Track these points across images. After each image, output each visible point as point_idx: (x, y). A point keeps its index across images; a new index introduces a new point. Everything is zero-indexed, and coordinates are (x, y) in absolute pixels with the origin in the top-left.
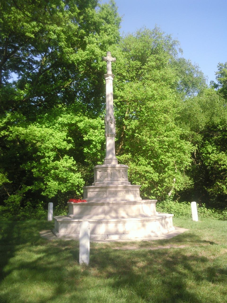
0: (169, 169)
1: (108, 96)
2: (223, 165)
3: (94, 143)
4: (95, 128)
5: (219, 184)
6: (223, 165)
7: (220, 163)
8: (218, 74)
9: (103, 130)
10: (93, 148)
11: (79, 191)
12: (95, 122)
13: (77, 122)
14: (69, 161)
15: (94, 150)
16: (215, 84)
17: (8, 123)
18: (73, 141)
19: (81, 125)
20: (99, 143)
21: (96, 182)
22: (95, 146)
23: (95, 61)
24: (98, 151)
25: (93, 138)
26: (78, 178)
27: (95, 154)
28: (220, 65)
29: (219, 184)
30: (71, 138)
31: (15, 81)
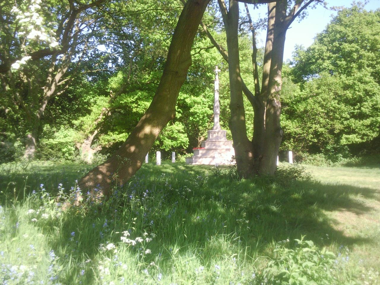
0: (249, 132)
1: (216, 102)
2: (289, 129)
3: (198, 114)
4: (198, 103)
5: (286, 143)
6: (289, 129)
7: (286, 128)
8: (294, 53)
9: (204, 105)
10: (197, 117)
11: (185, 146)
12: (198, 99)
13: (185, 98)
14: (179, 125)
15: (198, 119)
16: (291, 62)
17: (139, 99)
18: (182, 112)
19: (188, 101)
20: (201, 114)
21: (208, 140)
22: (198, 116)
23: (241, 171)
24: (200, 119)
25: (197, 111)
26: (185, 137)
27: (198, 122)
28: (297, 46)
29: (286, 143)
30: (180, 110)
31: (343, 232)
